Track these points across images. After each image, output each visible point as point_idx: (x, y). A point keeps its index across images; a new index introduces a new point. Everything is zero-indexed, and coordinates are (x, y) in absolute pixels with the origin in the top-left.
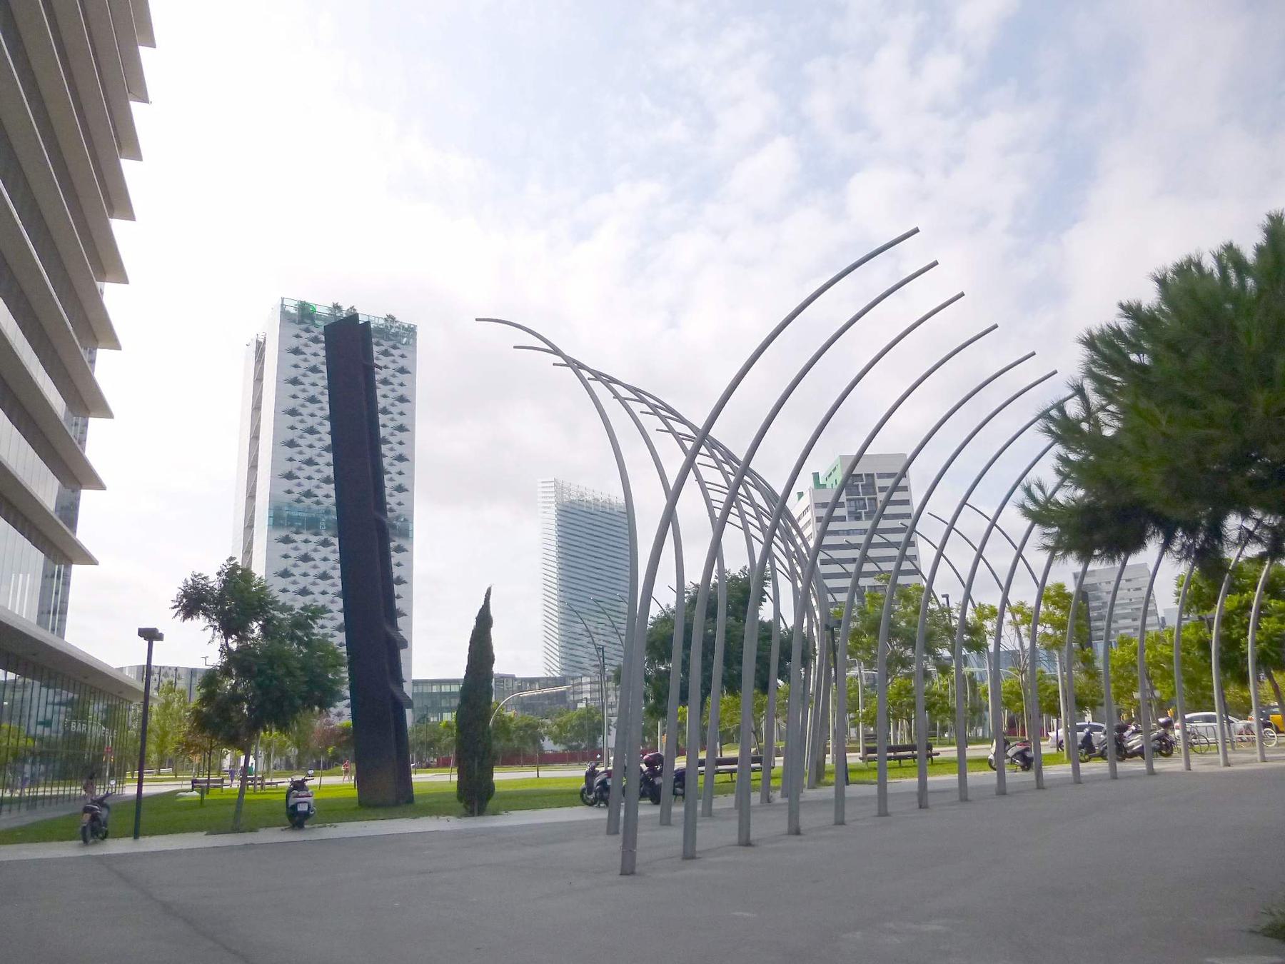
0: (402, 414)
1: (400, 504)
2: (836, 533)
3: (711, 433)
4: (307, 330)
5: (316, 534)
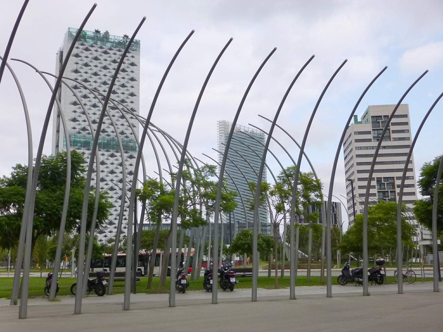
0: (132, 87)
2: (384, 147)
3: (84, 29)
5: (108, 151)
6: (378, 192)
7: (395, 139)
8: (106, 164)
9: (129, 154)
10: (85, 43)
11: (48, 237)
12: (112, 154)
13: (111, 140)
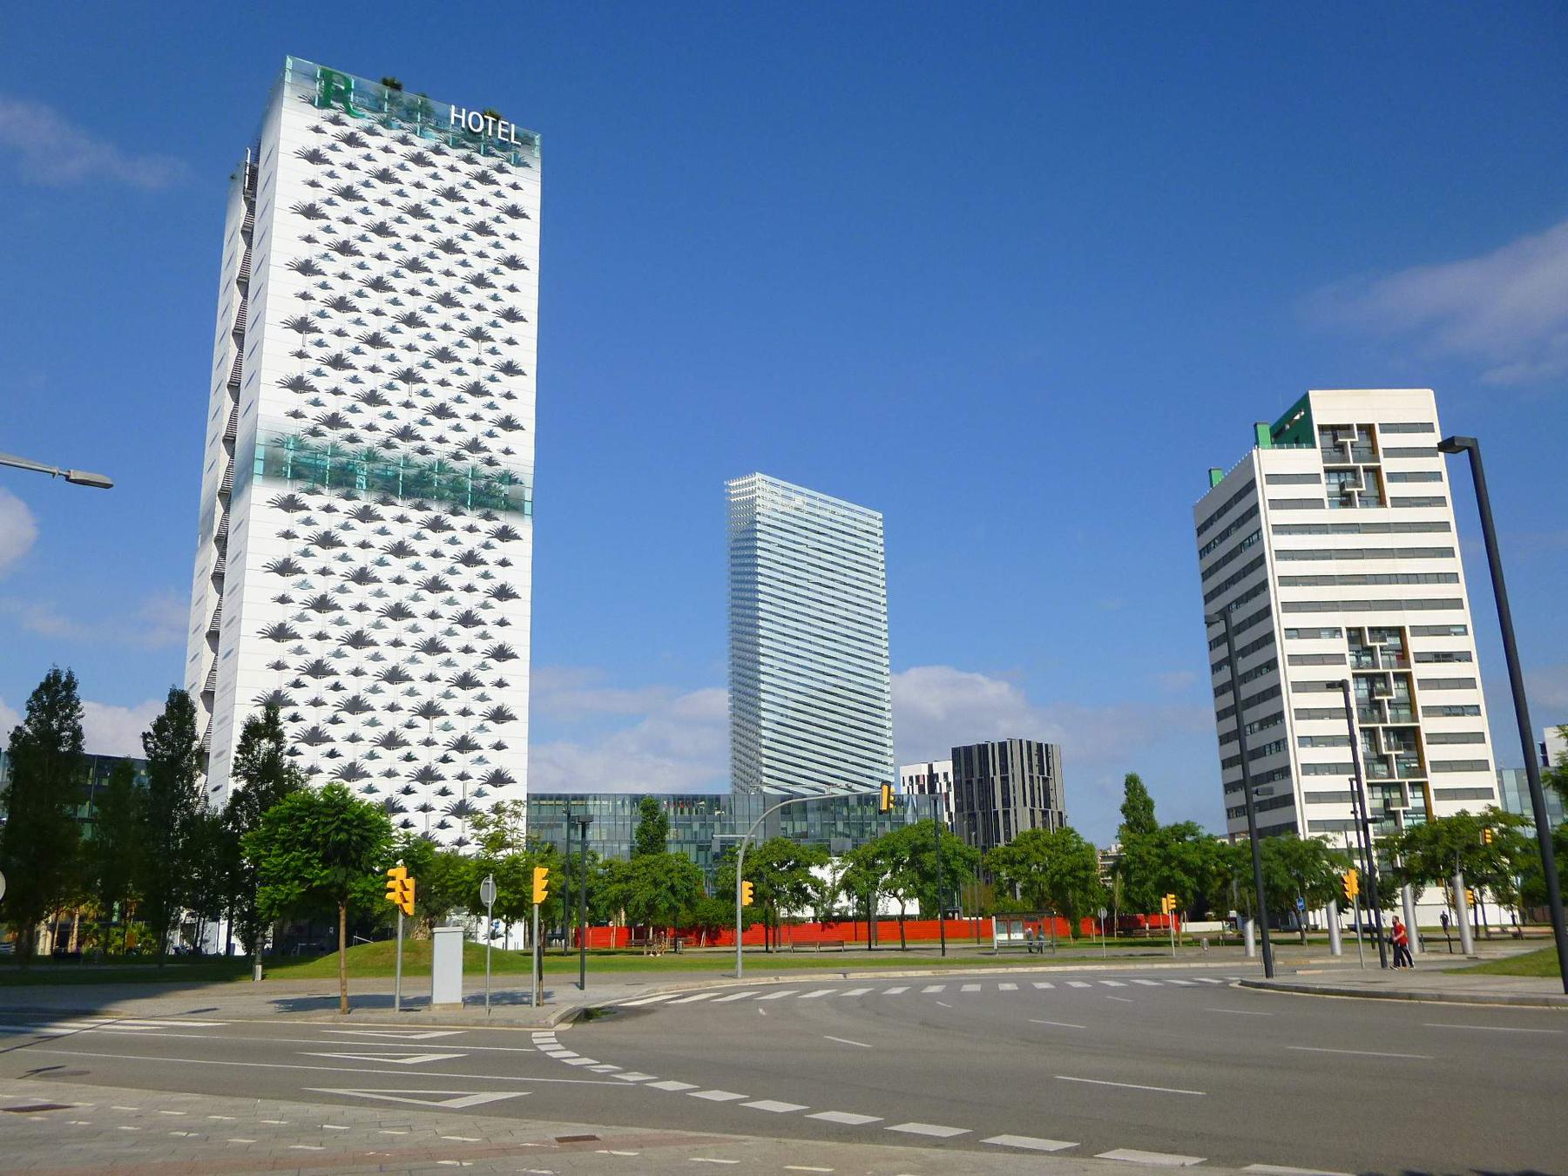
1: (507, 452)
4: (336, 121)
6: (1355, 675)
7: (1399, 502)
8: (480, 622)
9: (498, 525)
10: (345, 118)
11: (389, 896)
12: (438, 518)
13: (432, 469)
